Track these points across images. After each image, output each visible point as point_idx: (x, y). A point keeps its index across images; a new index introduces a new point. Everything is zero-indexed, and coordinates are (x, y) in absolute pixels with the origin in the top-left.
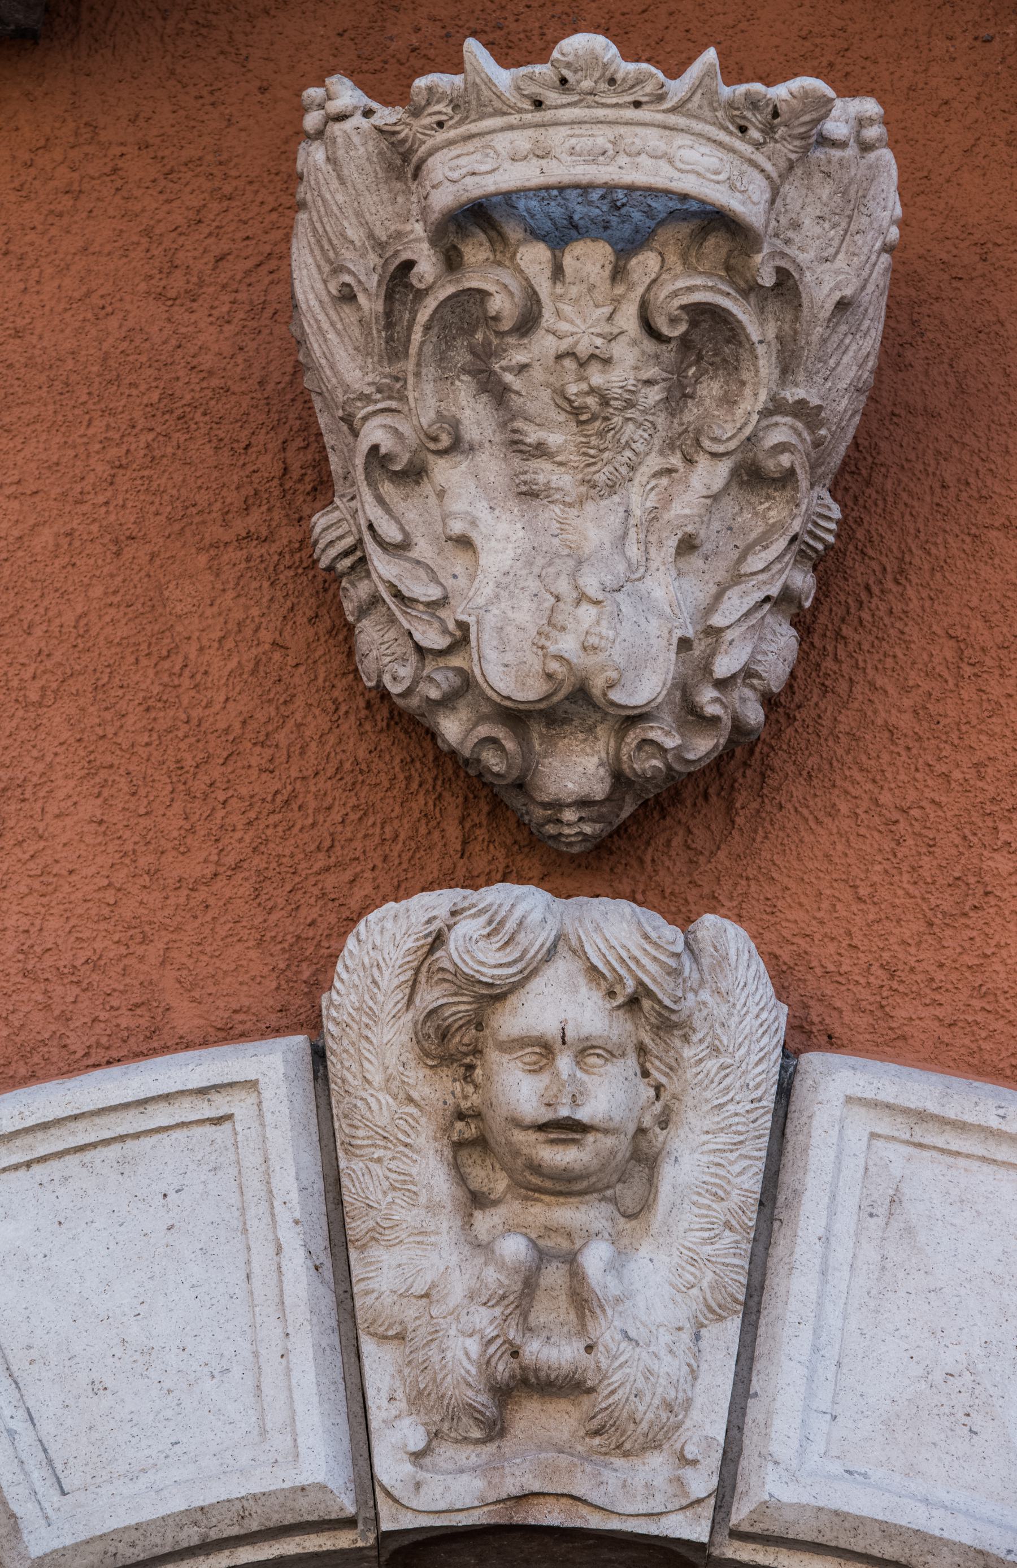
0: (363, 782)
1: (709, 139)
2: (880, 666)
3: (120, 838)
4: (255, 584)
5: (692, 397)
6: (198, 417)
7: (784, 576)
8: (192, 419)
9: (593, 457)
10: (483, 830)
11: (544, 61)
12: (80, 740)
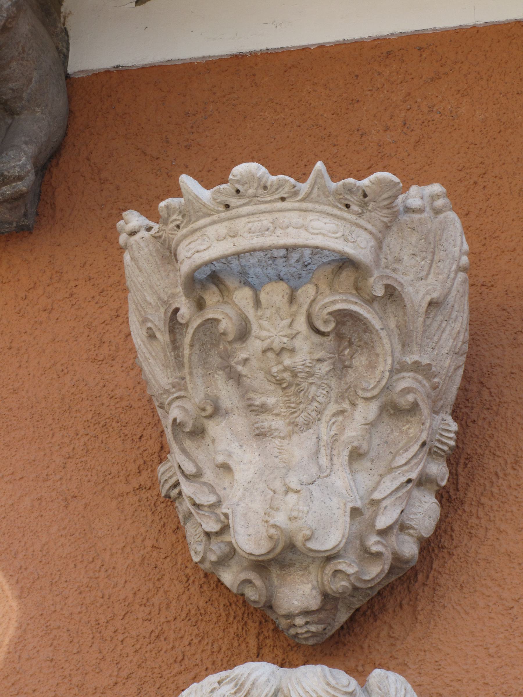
0: (202, 620)
1: (328, 214)
2: (503, 518)
3: (62, 668)
4: (144, 514)
5: (350, 367)
6: (114, 424)
7: (420, 467)
8: (111, 425)
9: (293, 408)
10: (270, 640)
11: (227, 182)
12: (42, 615)
